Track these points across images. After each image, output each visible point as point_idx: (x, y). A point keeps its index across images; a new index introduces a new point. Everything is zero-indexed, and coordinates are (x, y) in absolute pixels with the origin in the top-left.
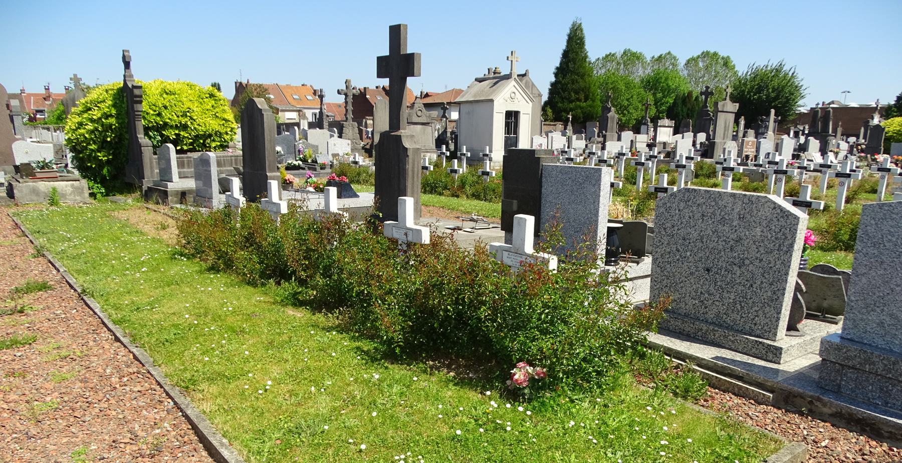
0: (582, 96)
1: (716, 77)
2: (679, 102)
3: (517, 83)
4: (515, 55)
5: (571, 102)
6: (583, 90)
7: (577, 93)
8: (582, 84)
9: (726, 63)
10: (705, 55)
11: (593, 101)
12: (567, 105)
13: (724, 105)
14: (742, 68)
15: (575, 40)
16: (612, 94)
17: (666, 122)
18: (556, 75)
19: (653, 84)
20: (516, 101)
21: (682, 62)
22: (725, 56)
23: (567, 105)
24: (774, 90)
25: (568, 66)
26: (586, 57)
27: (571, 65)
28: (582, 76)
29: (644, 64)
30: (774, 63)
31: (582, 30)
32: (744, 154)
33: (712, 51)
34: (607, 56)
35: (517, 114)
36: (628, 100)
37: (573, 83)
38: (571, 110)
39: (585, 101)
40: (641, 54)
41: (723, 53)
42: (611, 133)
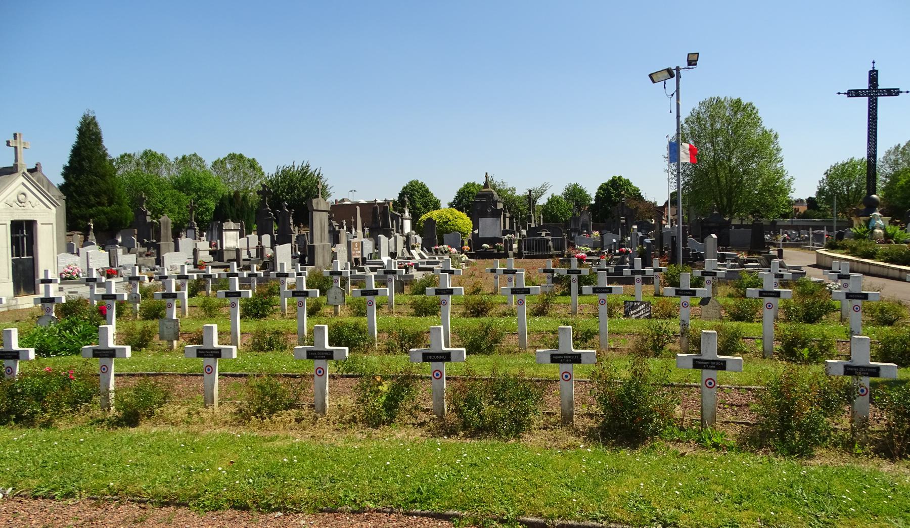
0: (105, 199)
1: (245, 178)
2: (227, 203)
3: (28, 179)
4: (22, 139)
5: (91, 206)
6: (105, 193)
7: (97, 195)
8: (103, 185)
9: (253, 164)
10: (232, 157)
11: (120, 205)
12: (84, 211)
13: (317, 203)
14: (270, 168)
15: (89, 137)
16: (140, 193)
17: (231, 225)
18: (65, 175)
19: (184, 185)
20: (28, 206)
21: (209, 164)
22: (251, 158)
23: (84, 211)
24: (304, 189)
25: (81, 165)
26: (105, 155)
27: (85, 164)
28: (103, 177)
29: (168, 166)
30: (298, 165)
31: (96, 124)
32: (353, 257)
33: (238, 153)
34: (122, 157)
35: (30, 225)
36: (160, 202)
37: (91, 185)
38: (92, 216)
39: (110, 206)
40: (162, 155)
41: (248, 155)
42: (166, 243)
